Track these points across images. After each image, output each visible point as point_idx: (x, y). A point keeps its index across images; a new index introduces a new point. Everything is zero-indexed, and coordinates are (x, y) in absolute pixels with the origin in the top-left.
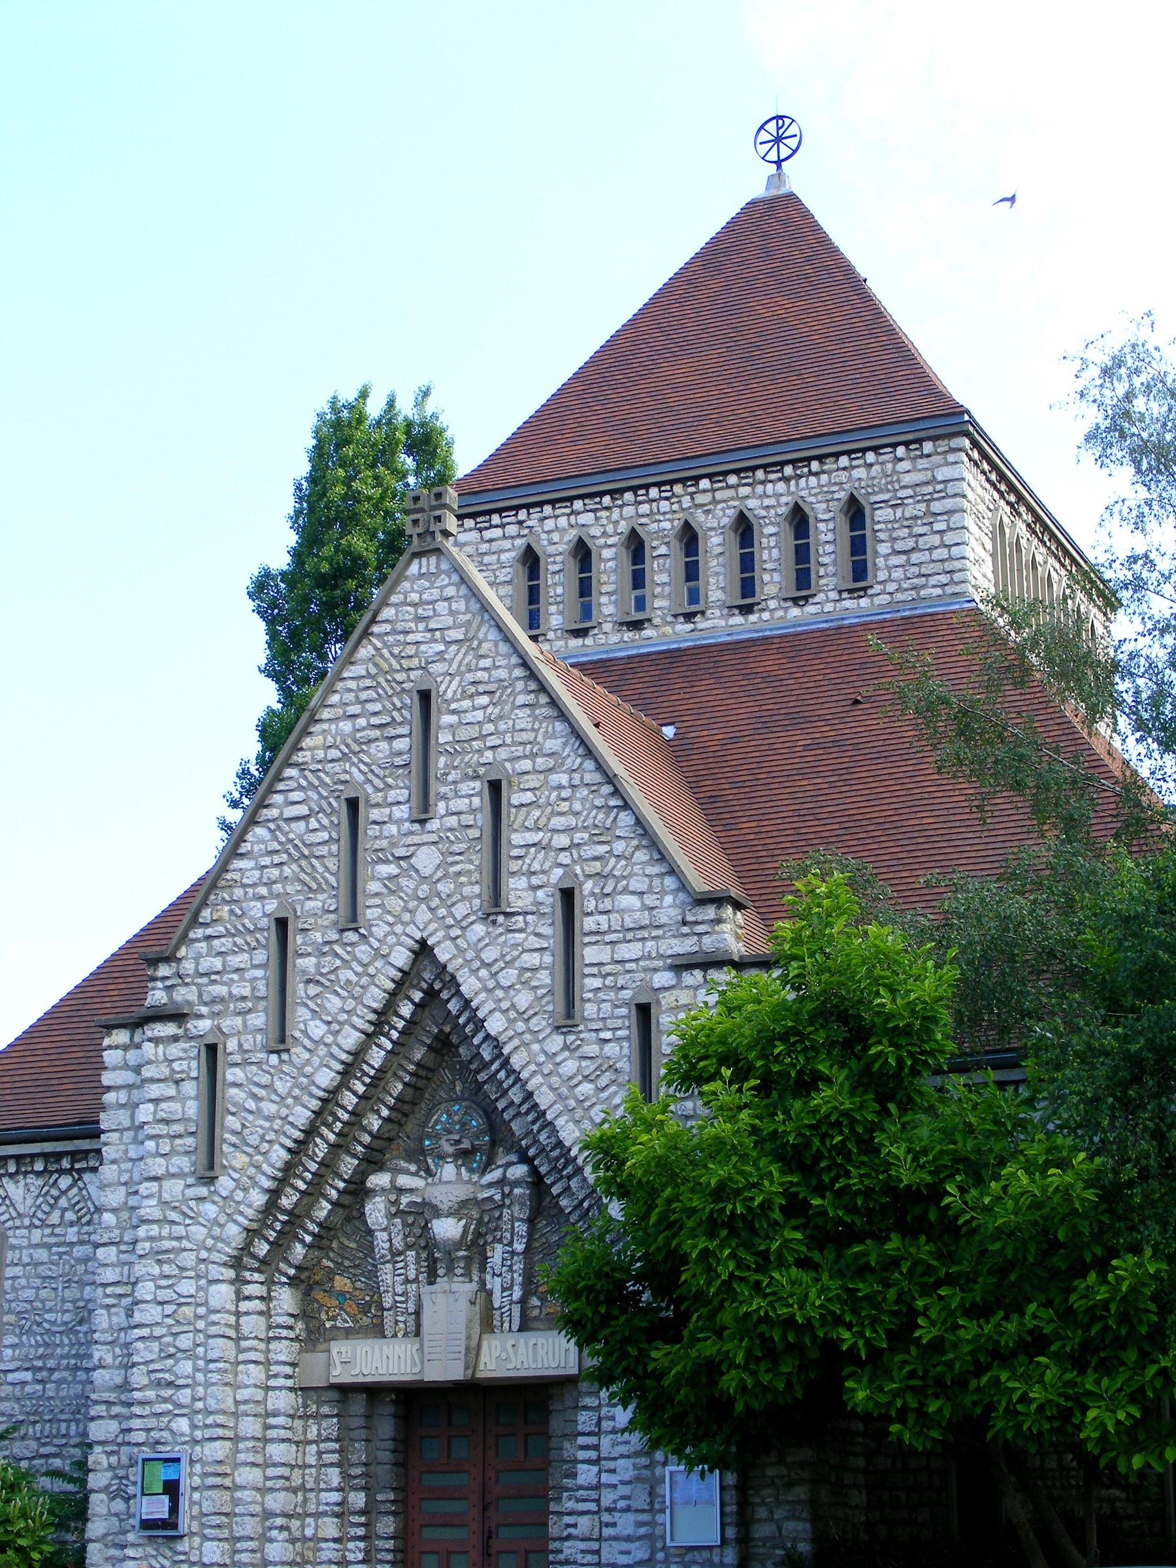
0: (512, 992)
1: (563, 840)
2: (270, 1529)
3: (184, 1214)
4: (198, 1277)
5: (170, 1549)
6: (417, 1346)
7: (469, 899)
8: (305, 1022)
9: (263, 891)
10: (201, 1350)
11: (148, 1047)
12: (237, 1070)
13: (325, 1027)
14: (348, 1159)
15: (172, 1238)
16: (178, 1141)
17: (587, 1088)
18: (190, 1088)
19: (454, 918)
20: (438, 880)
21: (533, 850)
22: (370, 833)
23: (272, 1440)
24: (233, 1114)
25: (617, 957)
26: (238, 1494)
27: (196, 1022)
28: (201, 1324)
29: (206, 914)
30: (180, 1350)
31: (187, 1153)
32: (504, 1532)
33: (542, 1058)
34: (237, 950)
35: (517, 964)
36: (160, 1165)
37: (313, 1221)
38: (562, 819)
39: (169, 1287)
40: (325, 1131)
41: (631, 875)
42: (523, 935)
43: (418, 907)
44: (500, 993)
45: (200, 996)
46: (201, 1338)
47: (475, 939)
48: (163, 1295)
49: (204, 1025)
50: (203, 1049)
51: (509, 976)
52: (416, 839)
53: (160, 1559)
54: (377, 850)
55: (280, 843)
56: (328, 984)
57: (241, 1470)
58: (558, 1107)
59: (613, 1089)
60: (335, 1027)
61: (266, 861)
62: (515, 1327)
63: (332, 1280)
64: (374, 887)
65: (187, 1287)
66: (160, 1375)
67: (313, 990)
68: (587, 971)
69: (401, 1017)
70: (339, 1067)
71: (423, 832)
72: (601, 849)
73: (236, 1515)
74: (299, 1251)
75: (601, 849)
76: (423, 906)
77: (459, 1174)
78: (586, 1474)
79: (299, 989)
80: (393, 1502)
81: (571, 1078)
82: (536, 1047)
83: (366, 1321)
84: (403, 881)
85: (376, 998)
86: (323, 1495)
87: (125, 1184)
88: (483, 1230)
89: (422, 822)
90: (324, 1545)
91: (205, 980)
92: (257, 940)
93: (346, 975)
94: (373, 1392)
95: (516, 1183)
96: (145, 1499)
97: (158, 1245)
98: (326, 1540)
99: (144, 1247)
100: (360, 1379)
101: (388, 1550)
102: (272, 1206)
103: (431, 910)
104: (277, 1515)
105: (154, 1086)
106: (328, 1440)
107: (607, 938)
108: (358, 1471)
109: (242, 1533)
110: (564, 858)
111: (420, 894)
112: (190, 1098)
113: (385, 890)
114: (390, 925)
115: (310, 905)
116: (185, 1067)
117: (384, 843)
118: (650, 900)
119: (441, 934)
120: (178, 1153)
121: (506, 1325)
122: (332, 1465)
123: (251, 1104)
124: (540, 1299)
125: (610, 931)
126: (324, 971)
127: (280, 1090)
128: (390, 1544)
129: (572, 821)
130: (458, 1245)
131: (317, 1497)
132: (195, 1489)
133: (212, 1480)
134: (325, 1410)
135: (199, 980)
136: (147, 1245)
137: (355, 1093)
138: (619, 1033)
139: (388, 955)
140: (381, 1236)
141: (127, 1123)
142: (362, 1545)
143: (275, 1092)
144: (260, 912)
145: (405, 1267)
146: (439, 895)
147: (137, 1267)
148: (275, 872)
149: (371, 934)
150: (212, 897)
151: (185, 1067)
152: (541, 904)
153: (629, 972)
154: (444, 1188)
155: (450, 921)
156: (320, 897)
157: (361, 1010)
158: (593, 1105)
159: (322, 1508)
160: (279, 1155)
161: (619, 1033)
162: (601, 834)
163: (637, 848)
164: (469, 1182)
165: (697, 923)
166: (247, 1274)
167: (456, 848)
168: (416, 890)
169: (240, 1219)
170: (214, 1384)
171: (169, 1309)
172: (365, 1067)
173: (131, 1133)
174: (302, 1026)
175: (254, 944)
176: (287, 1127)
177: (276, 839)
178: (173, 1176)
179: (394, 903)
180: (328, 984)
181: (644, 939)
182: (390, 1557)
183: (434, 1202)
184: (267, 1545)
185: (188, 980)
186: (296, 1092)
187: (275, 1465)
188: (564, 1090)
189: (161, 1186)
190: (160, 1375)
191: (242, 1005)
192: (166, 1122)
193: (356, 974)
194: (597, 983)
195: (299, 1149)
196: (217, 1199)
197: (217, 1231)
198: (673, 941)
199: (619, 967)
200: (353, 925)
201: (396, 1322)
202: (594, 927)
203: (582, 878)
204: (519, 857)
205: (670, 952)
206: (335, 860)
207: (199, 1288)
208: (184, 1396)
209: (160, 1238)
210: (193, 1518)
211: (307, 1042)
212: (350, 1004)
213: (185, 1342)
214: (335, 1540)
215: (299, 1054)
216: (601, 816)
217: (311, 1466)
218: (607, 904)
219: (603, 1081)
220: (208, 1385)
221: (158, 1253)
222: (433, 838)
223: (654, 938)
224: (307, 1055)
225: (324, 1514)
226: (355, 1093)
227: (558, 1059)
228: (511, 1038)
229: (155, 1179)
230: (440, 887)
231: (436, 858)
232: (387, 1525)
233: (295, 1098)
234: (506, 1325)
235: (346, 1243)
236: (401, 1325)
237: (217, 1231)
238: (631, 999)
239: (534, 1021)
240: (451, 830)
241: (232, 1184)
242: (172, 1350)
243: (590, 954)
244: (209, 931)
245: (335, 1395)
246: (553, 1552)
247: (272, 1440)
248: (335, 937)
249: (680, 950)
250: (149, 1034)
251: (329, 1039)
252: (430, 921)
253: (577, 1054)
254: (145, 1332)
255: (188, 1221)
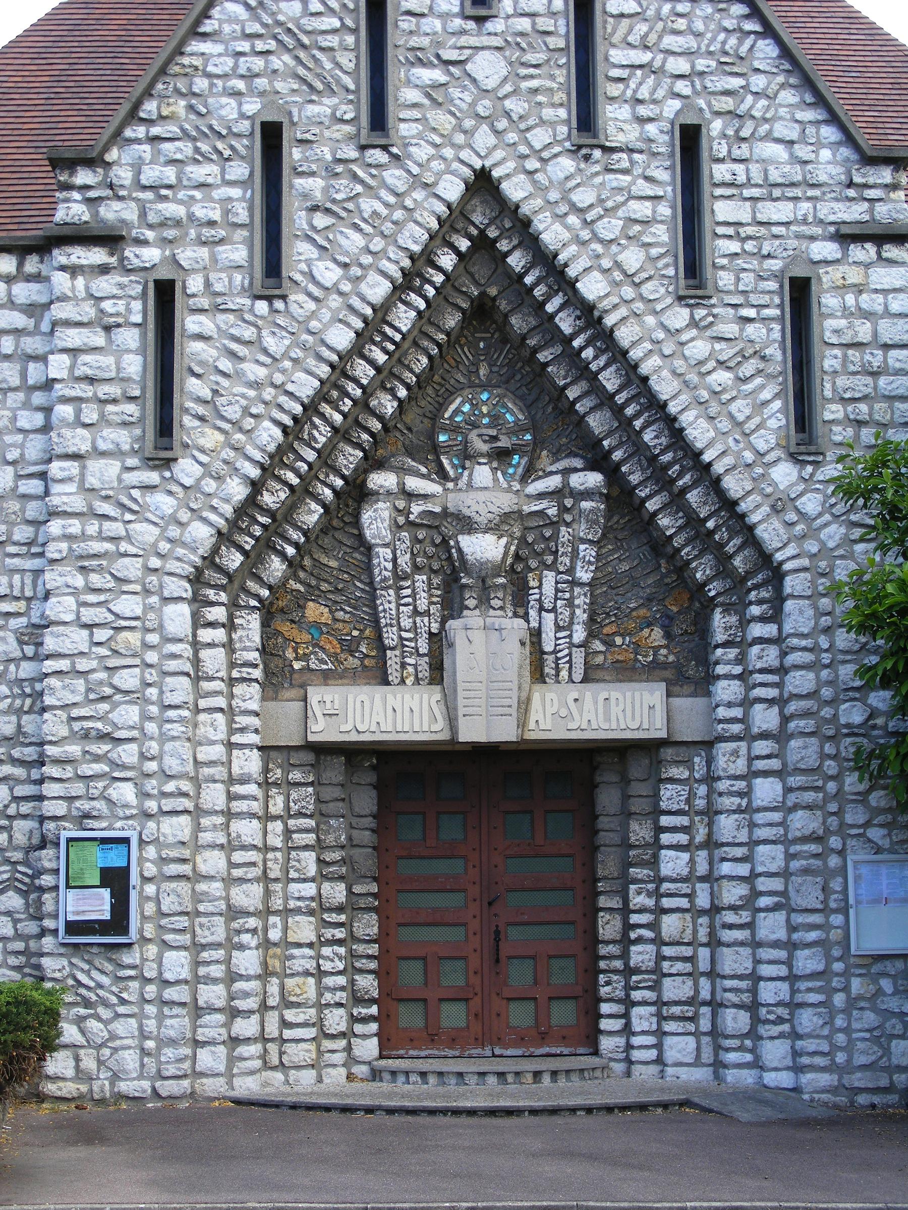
0: (614, 248)
1: (681, 65)
2: (239, 932)
3: (123, 506)
4: (147, 592)
5: (110, 960)
6: (438, 696)
7: (552, 124)
8: (309, 262)
9: (240, 85)
10: (152, 692)
11: (61, 280)
12: (202, 318)
13: (339, 271)
14: (349, 449)
15: (101, 537)
16: (110, 408)
17: (723, 377)
18: (129, 338)
19: (531, 147)
20: (506, 97)
21: (639, 73)
22: (404, 25)
23: (240, 815)
24: (198, 376)
25: (760, 217)
26: (202, 887)
27: (138, 250)
28: (152, 657)
29: (150, 108)
30: (118, 690)
31: (125, 424)
32: (514, 933)
33: (661, 335)
34: (198, 158)
35: (620, 213)
36: (83, 439)
37: (298, 528)
38: (680, 40)
39: (99, 604)
40: (326, 409)
41: (776, 118)
42: (628, 178)
43: (475, 129)
44: (598, 248)
45: (143, 214)
46: (152, 676)
47: (562, 176)
48: (88, 615)
49: (151, 255)
50: (151, 285)
51: (610, 228)
52: (473, 41)
53: (95, 974)
54: (413, 49)
55: (265, 25)
56: (344, 214)
57: (207, 854)
58: (684, 398)
59: (758, 381)
60: (356, 271)
61: (245, 46)
62: (578, 675)
63: (303, 607)
64: (411, 95)
65: (128, 605)
66: (90, 724)
67: (320, 220)
68: (720, 230)
69: (440, 269)
70: (359, 324)
71: (479, 34)
72: (735, 83)
73: (198, 914)
74: (276, 567)
75: (735, 83)
76: (485, 127)
77: (496, 480)
78: (673, 863)
79: (296, 217)
80: (375, 896)
81: (701, 363)
82: (650, 320)
83: (353, 662)
84: (455, 93)
85: (414, 238)
86: (294, 887)
87: (13, 463)
88: (524, 552)
89: (480, 20)
90: (296, 952)
91: (149, 195)
92: (232, 148)
93: (368, 205)
94: (352, 754)
95: (587, 494)
96: (71, 893)
97: (80, 547)
98: (299, 945)
99: (55, 550)
100: (354, 737)
101: (369, 957)
102: (251, 503)
103: (497, 133)
104: (249, 914)
105: (72, 332)
106: (300, 814)
107: (746, 193)
108: (336, 855)
109: (210, 939)
110: (682, 87)
111: (480, 110)
112: (128, 351)
113: (426, 101)
114: (436, 146)
115: (312, 110)
116: (121, 308)
117: (425, 42)
118: (803, 152)
119: (511, 165)
120: (109, 424)
121: (564, 674)
122: (306, 847)
123: (225, 364)
124: (604, 643)
125: (749, 183)
126: (339, 197)
127: (272, 349)
128: (373, 949)
129: (689, 42)
130: (497, 569)
131: (285, 889)
132: (146, 880)
133: (174, 869)
134: (296, 776)
135: (141, 195)
136: (64, 546)
137: (371, 362)
138: (767, 312)
139: (435, 184)
140: (385, 553)
141: (16, 381)
142: (342, 950)
143: (265, 352)
144: (236, 112)
145: (414, 595)
146: (507, 114)
147: (48, 576)
148: (258, 63)
149: (409, 156)
150: (160, 86)
151: (121, 308)
152: (651, 141)
153: (776, 237)
154: (481, 496)
155: (523, 149)
156: (326, 101)
157: (392, 252)
158: (733, 399)
159: (292, 904)
160: (270, 435)
161: (767, 312)
162: (729, 63)
163: (782, 86)
164: (509, 490)
165: (866, 186)
166: (211, 593)
167: (530, 58)
168: (473, 105)
169: (213, 517)
170: (174, 738)
171: (101, 635)
172: (388, 331)
173: (21, 396)
174: (303, 267)
175: (227, 153)
176: (283, 399)
177: (258, 19)
178: (103, 454)
179: (442, 119)
180: (344, 214)
181: (796, 199)
182: (373, 965)
183: (466, 512)
184: (235, 953)
185: (122, 193)
186: (297, 353)
187: (244, 848)
188: (693, 377)
189: (84, 467)
190: (90, 724)
191: (207, 232)
192: (91, 380)
193: (387, 205)
194: (734, 247)
195: (293, 432)
196: (175, 488)
197: (174, 532)
198: (837, 206)
199: (763, 231)
200: (383, 142)
201: (403, 665)
202: (728, 178)
203: (708, 115)
204: (620, 80)
205: (832, 218)
206: (352, 55)
207: (148, 608)
208: (128, 754)
209: (84, 537)
210: (144, 918)
211: (312, 288)
212: (377, 244)
213: (128, 679)
214: (310, 945)
215: (300, 303)
216: (733, 41)
217: (275, 849)
218: (743, 151)
219: (748, 369)
220: (164, 738)
221: (81, 557)
222: (497, 42)
223: (809, 199)
224: (311, 306)
225: (298, 911)
226: (371, 362)
227: (684, 337)
228: (615, 307)
229: (76, 457)
230: (508, 104)
231: (502, 69)
232: (368, 925)
233: (295, 361)
234: (564, 674)
235: (325, 560)
236: (411, 669)
237: (174, 532)
238: (782, 271)
239: (649, 286)
240: (522, 34)
241: (198, 470)
242: (108, 691)
243: (724, 210)
244: (155, 131)
245: (310, 757)
246: (604, 958)
247: (240, 815)
248: (353, 154)
249: (847, 217)
250: (63, 260)
251: (346, 287)
252: (495, 147)
253: (708, 333)
254: (63, 664)
255: (128, 517)
